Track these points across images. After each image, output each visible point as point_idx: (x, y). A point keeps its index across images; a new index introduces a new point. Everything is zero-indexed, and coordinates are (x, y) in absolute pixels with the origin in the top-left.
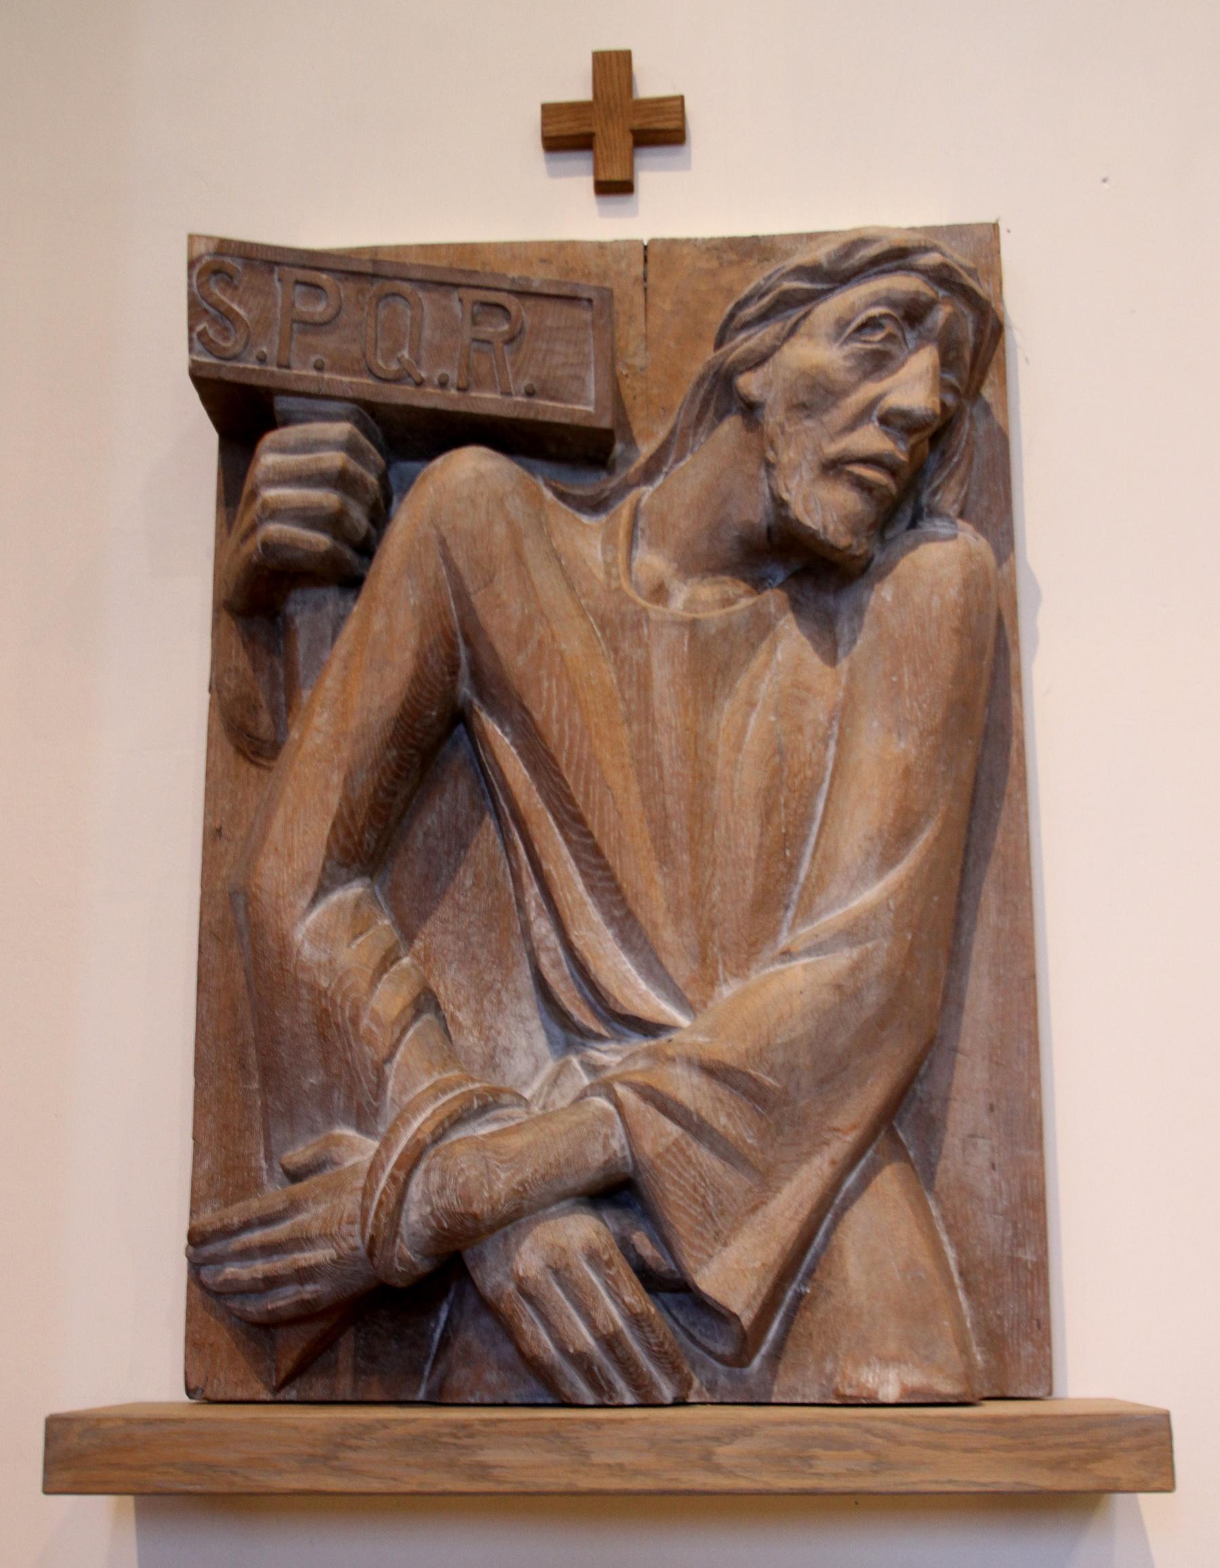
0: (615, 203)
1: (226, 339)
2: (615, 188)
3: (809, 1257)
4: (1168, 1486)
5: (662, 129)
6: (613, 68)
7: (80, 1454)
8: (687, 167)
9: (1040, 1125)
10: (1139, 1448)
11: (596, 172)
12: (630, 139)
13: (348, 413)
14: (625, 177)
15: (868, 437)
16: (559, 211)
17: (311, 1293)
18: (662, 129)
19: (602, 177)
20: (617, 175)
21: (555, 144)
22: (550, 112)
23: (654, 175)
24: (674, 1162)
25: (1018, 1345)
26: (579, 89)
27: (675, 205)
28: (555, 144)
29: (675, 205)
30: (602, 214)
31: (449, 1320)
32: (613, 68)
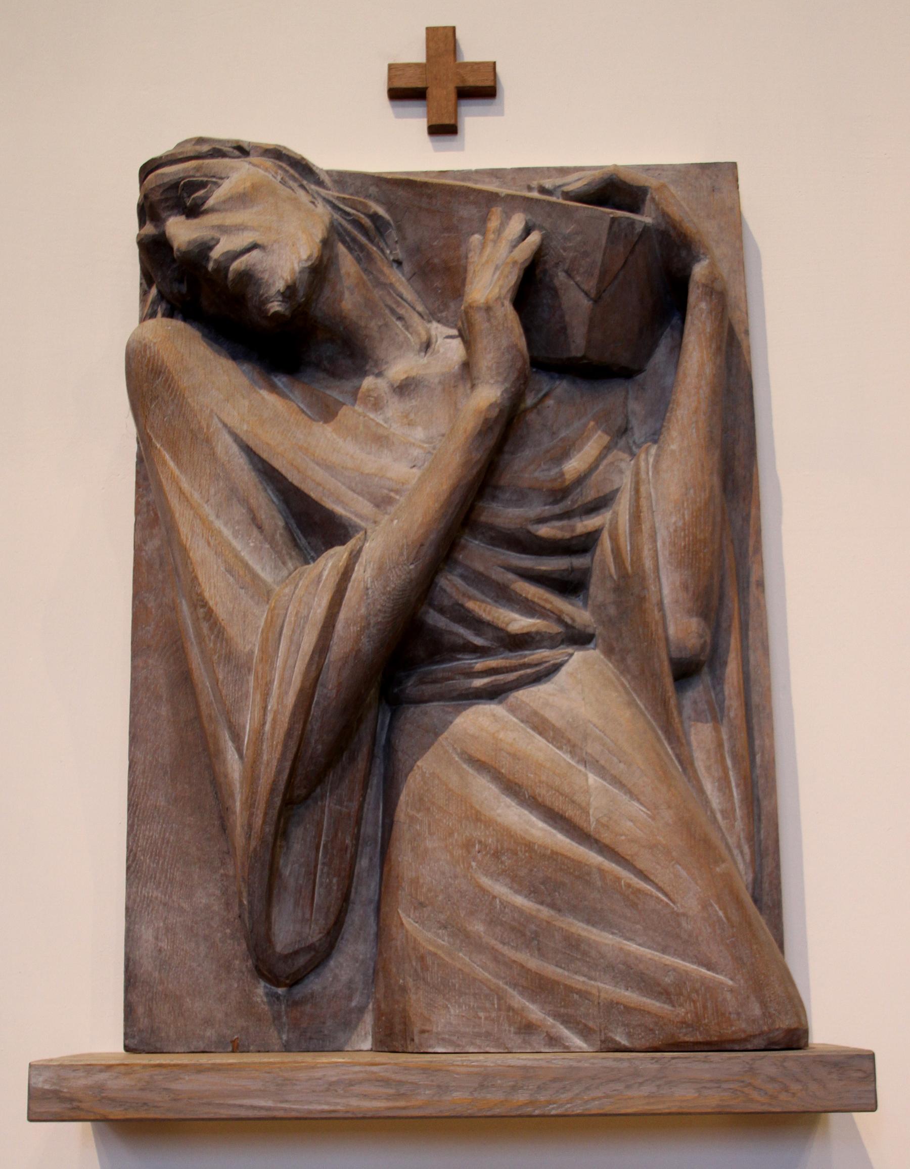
0: (445, 141)
2: (444, 129)
4: (872, 1106)
5: (481, 89)
6: (442, 41)
7: (54, 1097)
8: (501, 113)
9: (774, 780)
10: (854, 1079)
12: (453, 96)
14: (452, 122)
15: (633, 294)
16: (402, 148)
19: (436, 121)
21: (397, 95)
23: (474, 120)
25: (777, 1030)
26: (416, 54)
27: (487, 146)
28: (397, 95)
30: (436, 150)
32: (442, 41)
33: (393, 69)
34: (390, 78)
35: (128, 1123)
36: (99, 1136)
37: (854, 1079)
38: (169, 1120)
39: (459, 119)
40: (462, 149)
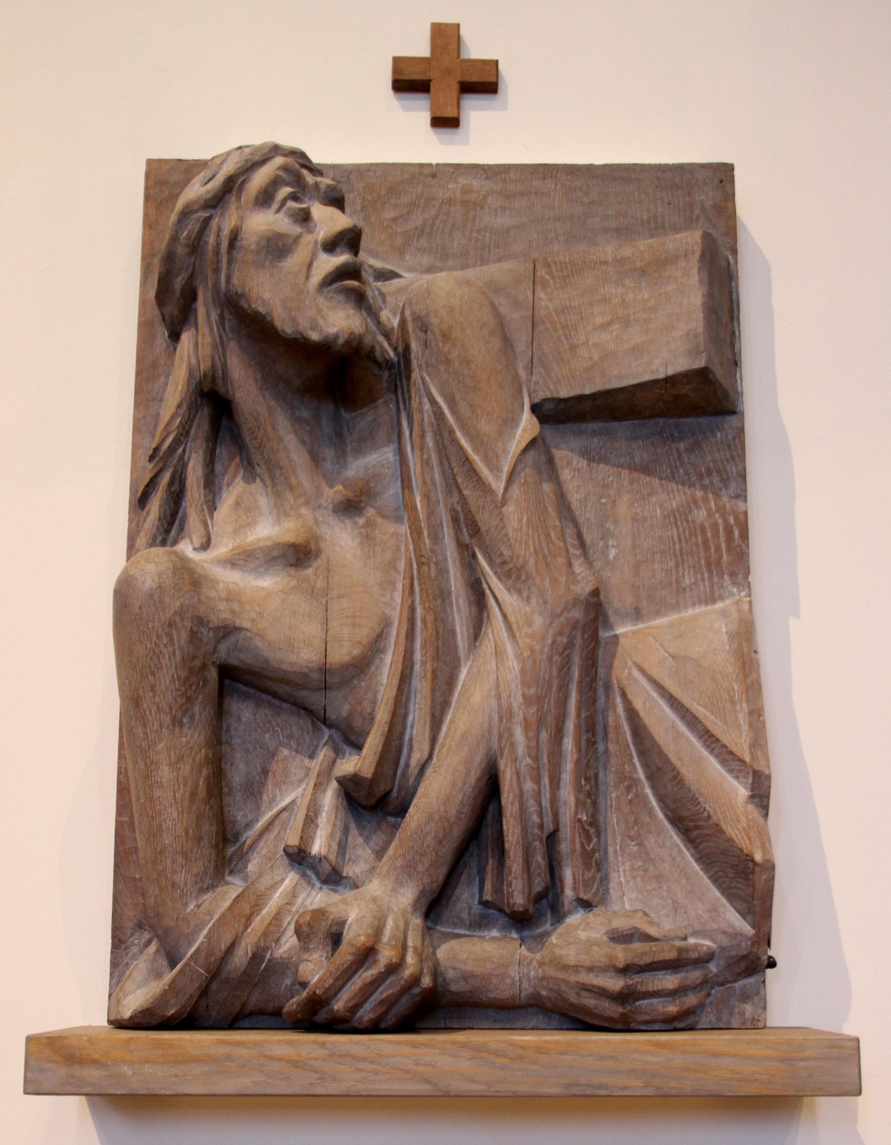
1: (421, 680)
3: (399, 772)
5: (483, 83)
6: (445, 36)
7: (53, 1063)
10: (836, 1068)
11: (432, 110)
12: (456, 88)
13: (266, 345)
14: (455, 115)
16: (403, 137)
17: (511, 867)
18: (483, 83)
19: (439, 114)
20: (450, 113)
22: (398, 62)
23: (476, 113)
24: (175, 637)
26: (421, 49)
27: (491, 137)
29: (491, 137)
31: (574, 844)
32: (445, 36)
33: (397, 61)
34: (395, 71)
35: (123, 1103)
36: (93, 1107)
37: (836, 1068)
38: (166, 1095)
39: (461, 112)
40: (466, 142)
